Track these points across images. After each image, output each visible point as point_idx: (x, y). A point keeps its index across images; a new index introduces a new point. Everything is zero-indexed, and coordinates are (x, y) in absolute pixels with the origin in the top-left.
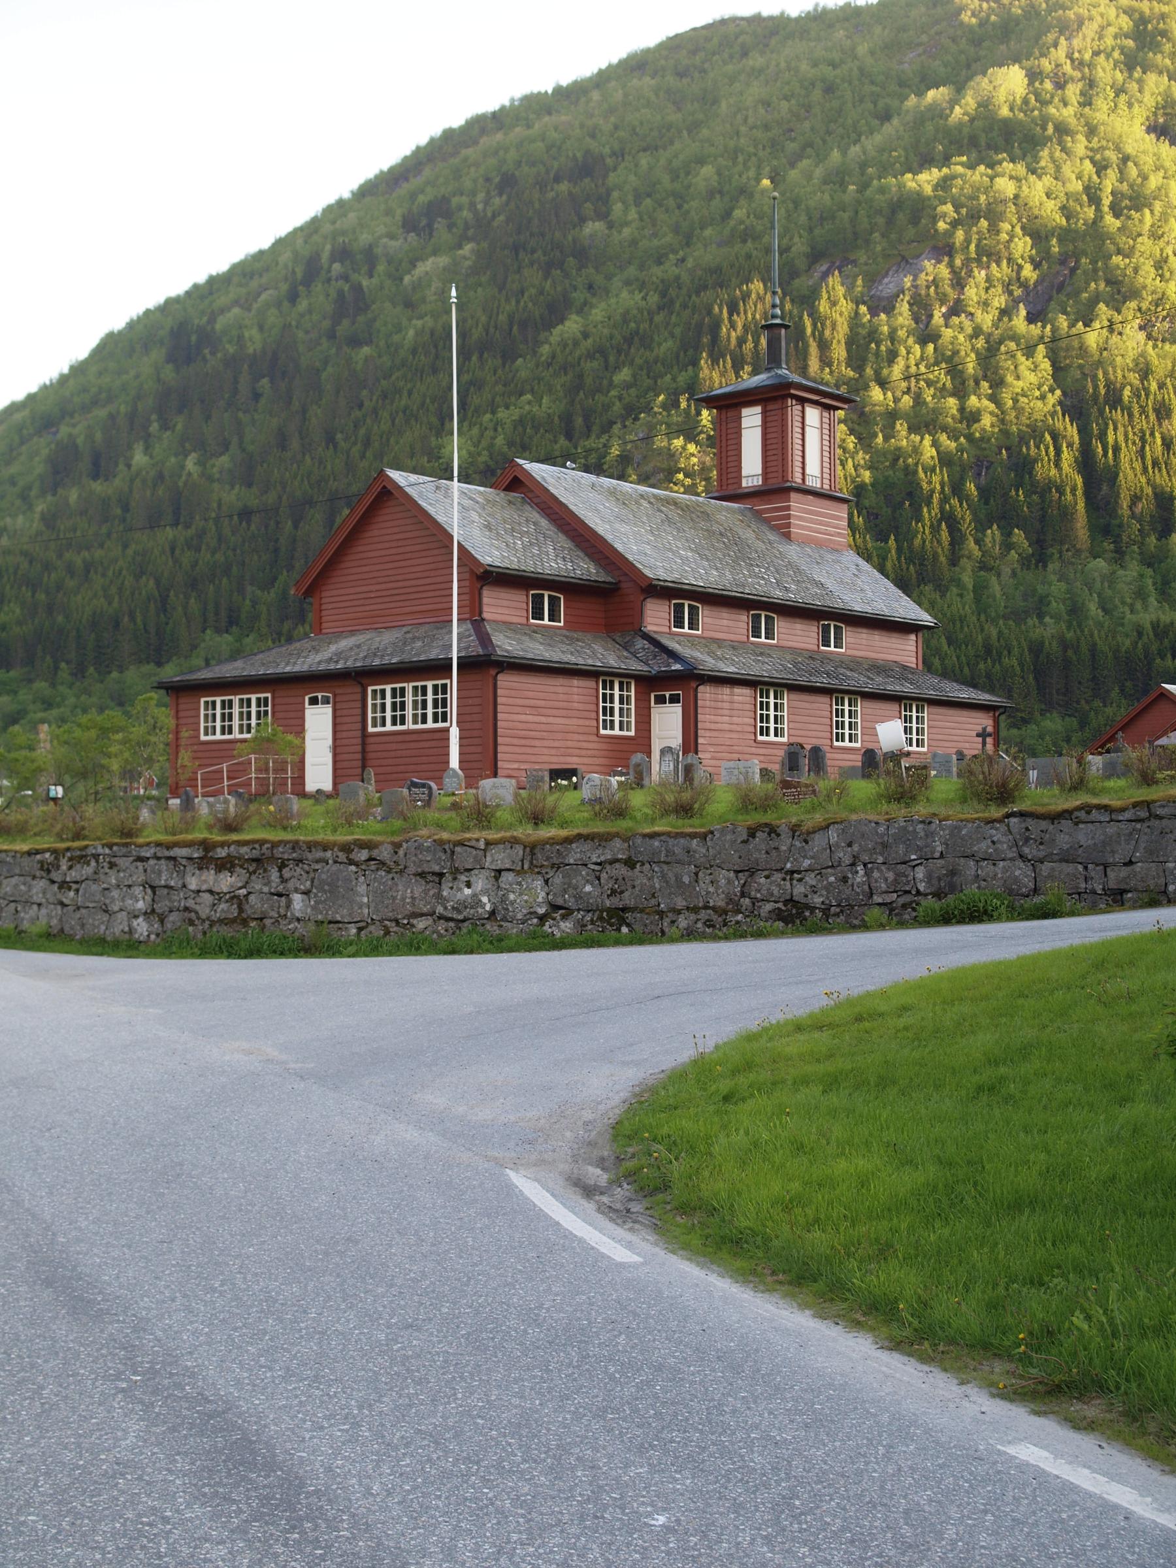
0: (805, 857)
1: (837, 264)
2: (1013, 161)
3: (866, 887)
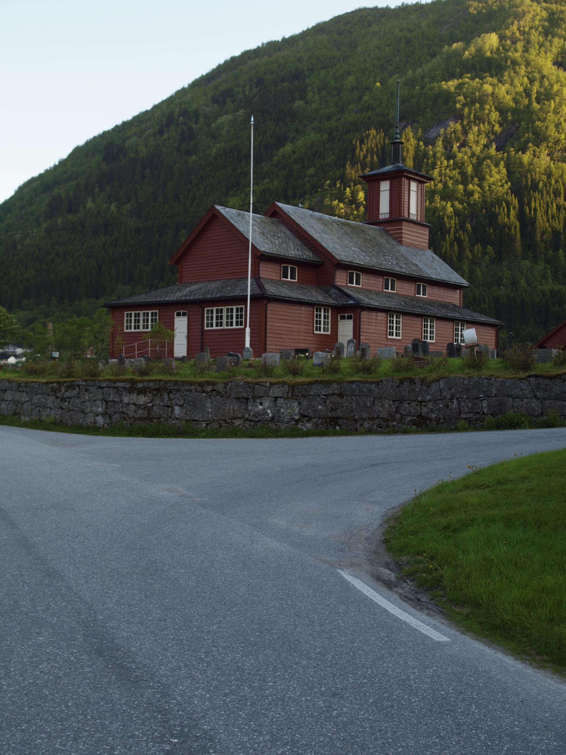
0: (428, 394)
1: (410, 122)
2: (491, 76)
3: (458, 410)
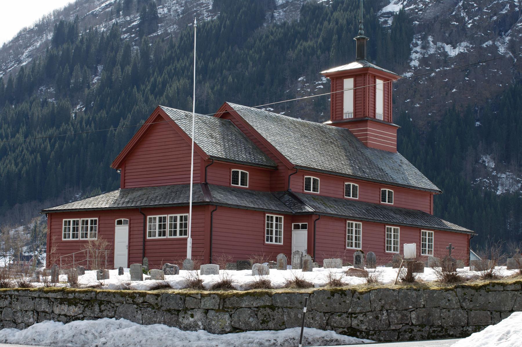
3: (387, 321)
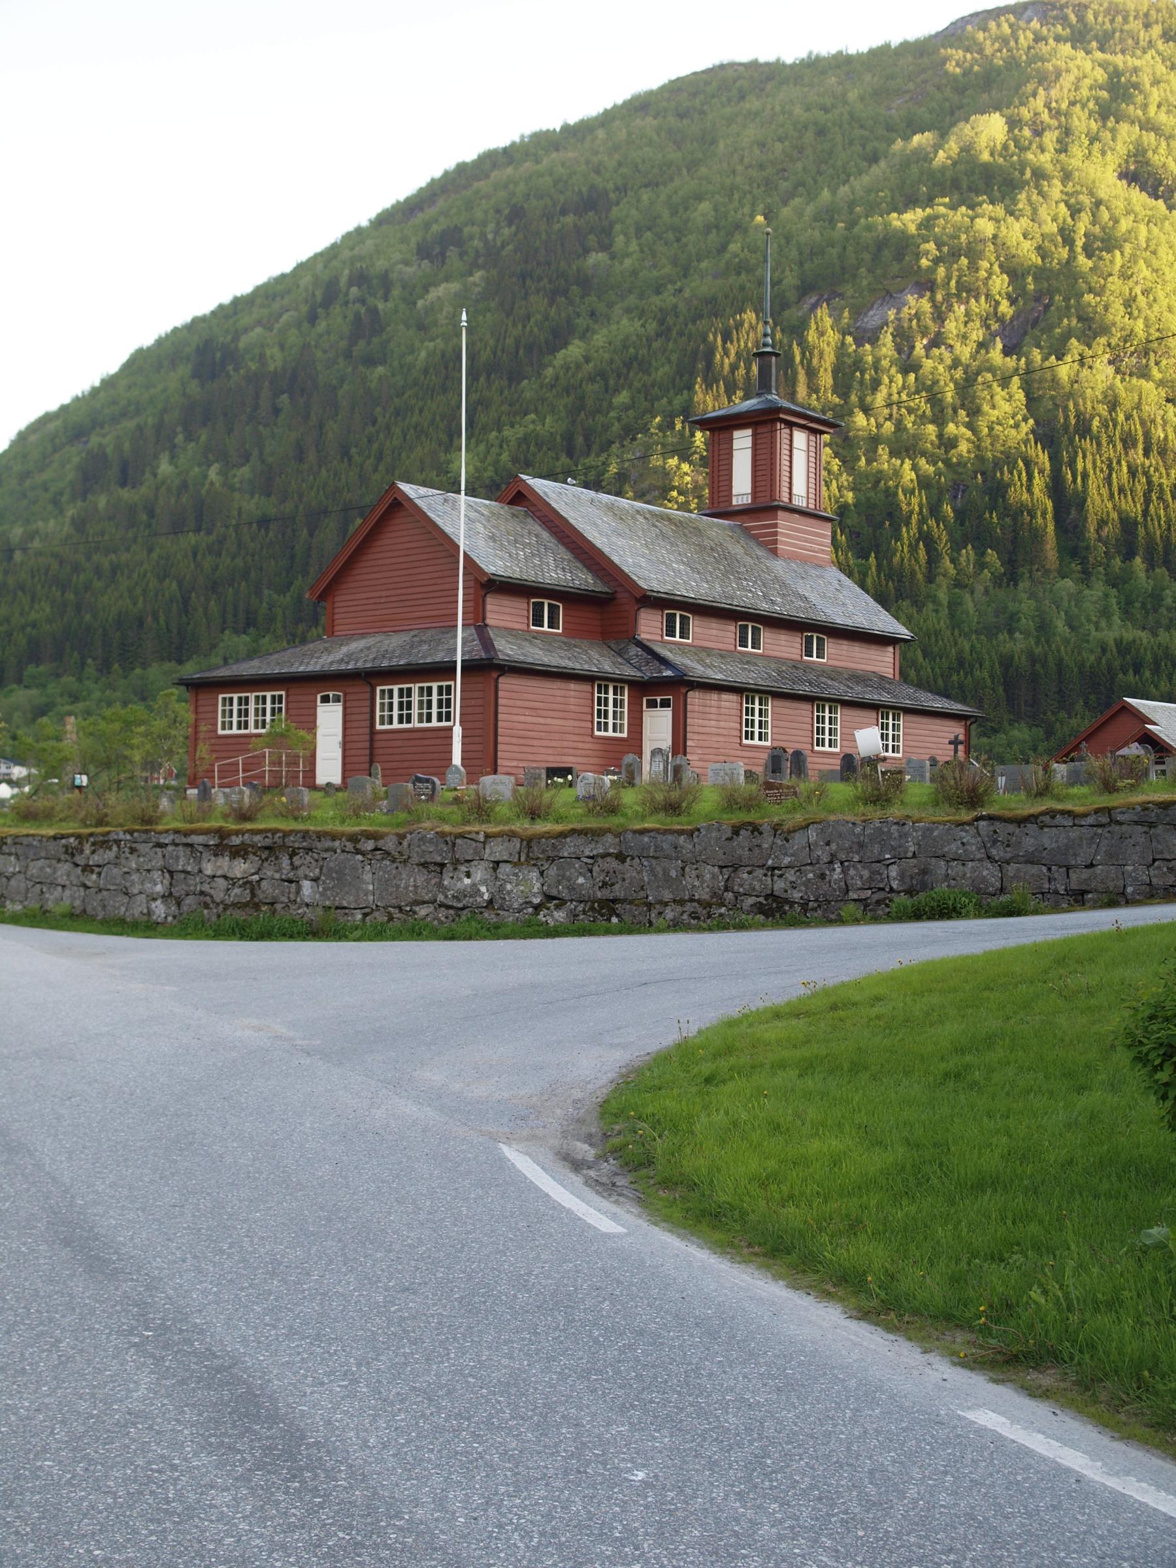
0: (785, 854)
2: (992, 203)
3: (842, 884)
